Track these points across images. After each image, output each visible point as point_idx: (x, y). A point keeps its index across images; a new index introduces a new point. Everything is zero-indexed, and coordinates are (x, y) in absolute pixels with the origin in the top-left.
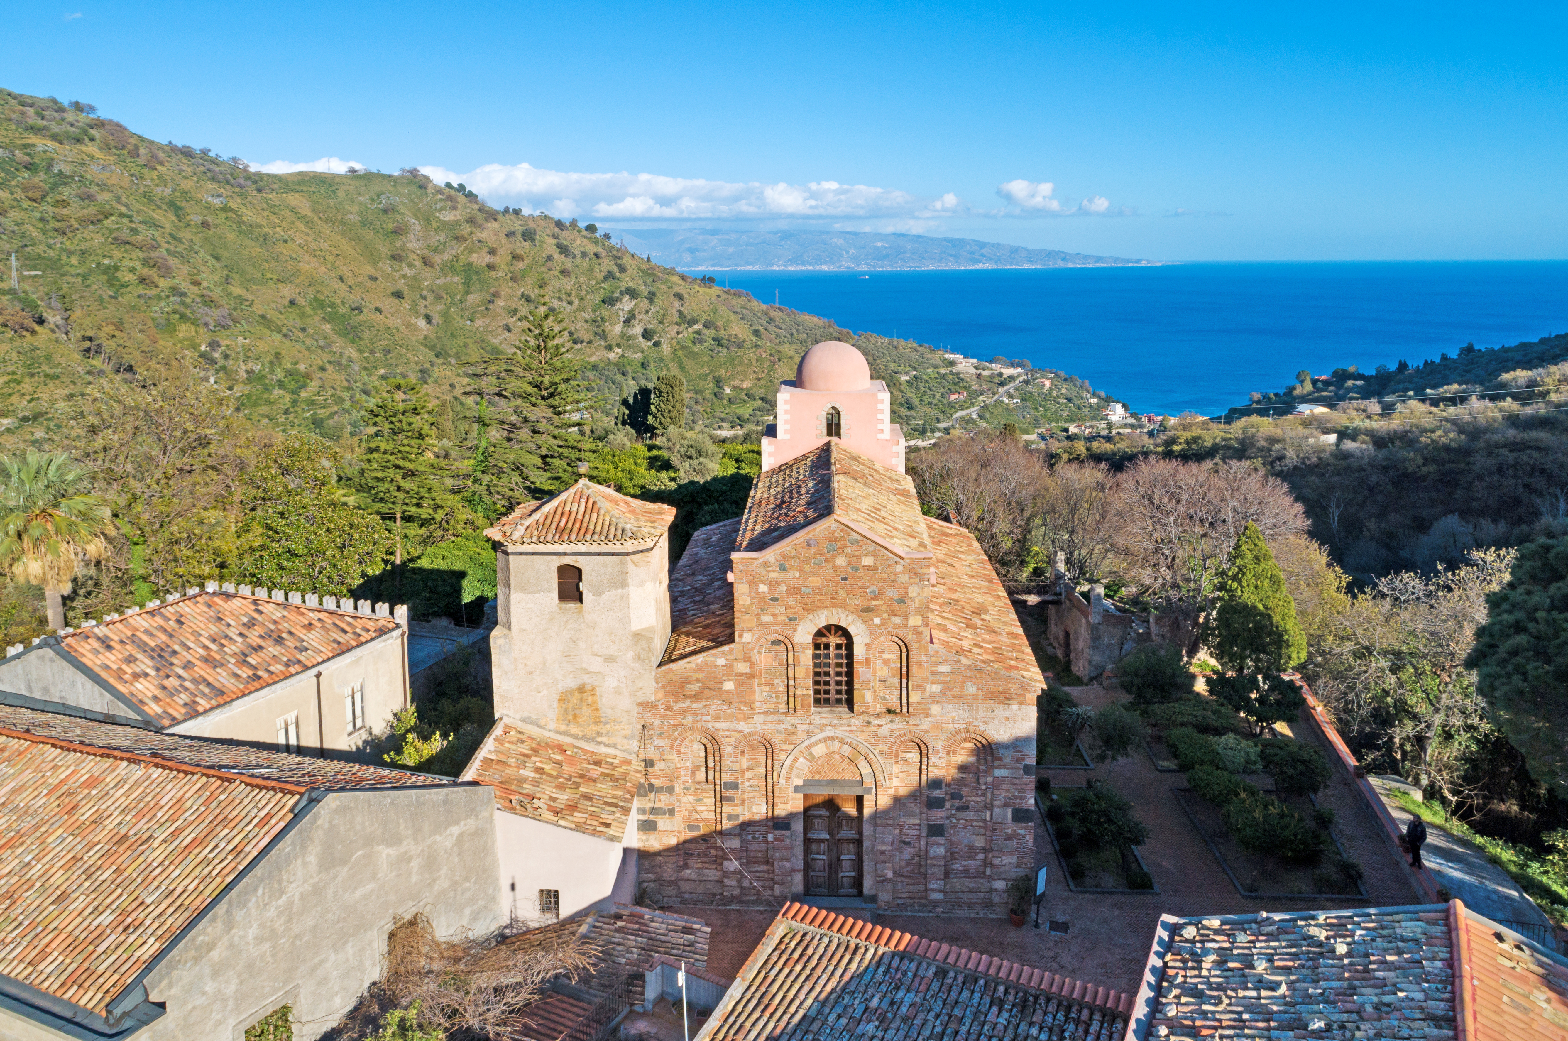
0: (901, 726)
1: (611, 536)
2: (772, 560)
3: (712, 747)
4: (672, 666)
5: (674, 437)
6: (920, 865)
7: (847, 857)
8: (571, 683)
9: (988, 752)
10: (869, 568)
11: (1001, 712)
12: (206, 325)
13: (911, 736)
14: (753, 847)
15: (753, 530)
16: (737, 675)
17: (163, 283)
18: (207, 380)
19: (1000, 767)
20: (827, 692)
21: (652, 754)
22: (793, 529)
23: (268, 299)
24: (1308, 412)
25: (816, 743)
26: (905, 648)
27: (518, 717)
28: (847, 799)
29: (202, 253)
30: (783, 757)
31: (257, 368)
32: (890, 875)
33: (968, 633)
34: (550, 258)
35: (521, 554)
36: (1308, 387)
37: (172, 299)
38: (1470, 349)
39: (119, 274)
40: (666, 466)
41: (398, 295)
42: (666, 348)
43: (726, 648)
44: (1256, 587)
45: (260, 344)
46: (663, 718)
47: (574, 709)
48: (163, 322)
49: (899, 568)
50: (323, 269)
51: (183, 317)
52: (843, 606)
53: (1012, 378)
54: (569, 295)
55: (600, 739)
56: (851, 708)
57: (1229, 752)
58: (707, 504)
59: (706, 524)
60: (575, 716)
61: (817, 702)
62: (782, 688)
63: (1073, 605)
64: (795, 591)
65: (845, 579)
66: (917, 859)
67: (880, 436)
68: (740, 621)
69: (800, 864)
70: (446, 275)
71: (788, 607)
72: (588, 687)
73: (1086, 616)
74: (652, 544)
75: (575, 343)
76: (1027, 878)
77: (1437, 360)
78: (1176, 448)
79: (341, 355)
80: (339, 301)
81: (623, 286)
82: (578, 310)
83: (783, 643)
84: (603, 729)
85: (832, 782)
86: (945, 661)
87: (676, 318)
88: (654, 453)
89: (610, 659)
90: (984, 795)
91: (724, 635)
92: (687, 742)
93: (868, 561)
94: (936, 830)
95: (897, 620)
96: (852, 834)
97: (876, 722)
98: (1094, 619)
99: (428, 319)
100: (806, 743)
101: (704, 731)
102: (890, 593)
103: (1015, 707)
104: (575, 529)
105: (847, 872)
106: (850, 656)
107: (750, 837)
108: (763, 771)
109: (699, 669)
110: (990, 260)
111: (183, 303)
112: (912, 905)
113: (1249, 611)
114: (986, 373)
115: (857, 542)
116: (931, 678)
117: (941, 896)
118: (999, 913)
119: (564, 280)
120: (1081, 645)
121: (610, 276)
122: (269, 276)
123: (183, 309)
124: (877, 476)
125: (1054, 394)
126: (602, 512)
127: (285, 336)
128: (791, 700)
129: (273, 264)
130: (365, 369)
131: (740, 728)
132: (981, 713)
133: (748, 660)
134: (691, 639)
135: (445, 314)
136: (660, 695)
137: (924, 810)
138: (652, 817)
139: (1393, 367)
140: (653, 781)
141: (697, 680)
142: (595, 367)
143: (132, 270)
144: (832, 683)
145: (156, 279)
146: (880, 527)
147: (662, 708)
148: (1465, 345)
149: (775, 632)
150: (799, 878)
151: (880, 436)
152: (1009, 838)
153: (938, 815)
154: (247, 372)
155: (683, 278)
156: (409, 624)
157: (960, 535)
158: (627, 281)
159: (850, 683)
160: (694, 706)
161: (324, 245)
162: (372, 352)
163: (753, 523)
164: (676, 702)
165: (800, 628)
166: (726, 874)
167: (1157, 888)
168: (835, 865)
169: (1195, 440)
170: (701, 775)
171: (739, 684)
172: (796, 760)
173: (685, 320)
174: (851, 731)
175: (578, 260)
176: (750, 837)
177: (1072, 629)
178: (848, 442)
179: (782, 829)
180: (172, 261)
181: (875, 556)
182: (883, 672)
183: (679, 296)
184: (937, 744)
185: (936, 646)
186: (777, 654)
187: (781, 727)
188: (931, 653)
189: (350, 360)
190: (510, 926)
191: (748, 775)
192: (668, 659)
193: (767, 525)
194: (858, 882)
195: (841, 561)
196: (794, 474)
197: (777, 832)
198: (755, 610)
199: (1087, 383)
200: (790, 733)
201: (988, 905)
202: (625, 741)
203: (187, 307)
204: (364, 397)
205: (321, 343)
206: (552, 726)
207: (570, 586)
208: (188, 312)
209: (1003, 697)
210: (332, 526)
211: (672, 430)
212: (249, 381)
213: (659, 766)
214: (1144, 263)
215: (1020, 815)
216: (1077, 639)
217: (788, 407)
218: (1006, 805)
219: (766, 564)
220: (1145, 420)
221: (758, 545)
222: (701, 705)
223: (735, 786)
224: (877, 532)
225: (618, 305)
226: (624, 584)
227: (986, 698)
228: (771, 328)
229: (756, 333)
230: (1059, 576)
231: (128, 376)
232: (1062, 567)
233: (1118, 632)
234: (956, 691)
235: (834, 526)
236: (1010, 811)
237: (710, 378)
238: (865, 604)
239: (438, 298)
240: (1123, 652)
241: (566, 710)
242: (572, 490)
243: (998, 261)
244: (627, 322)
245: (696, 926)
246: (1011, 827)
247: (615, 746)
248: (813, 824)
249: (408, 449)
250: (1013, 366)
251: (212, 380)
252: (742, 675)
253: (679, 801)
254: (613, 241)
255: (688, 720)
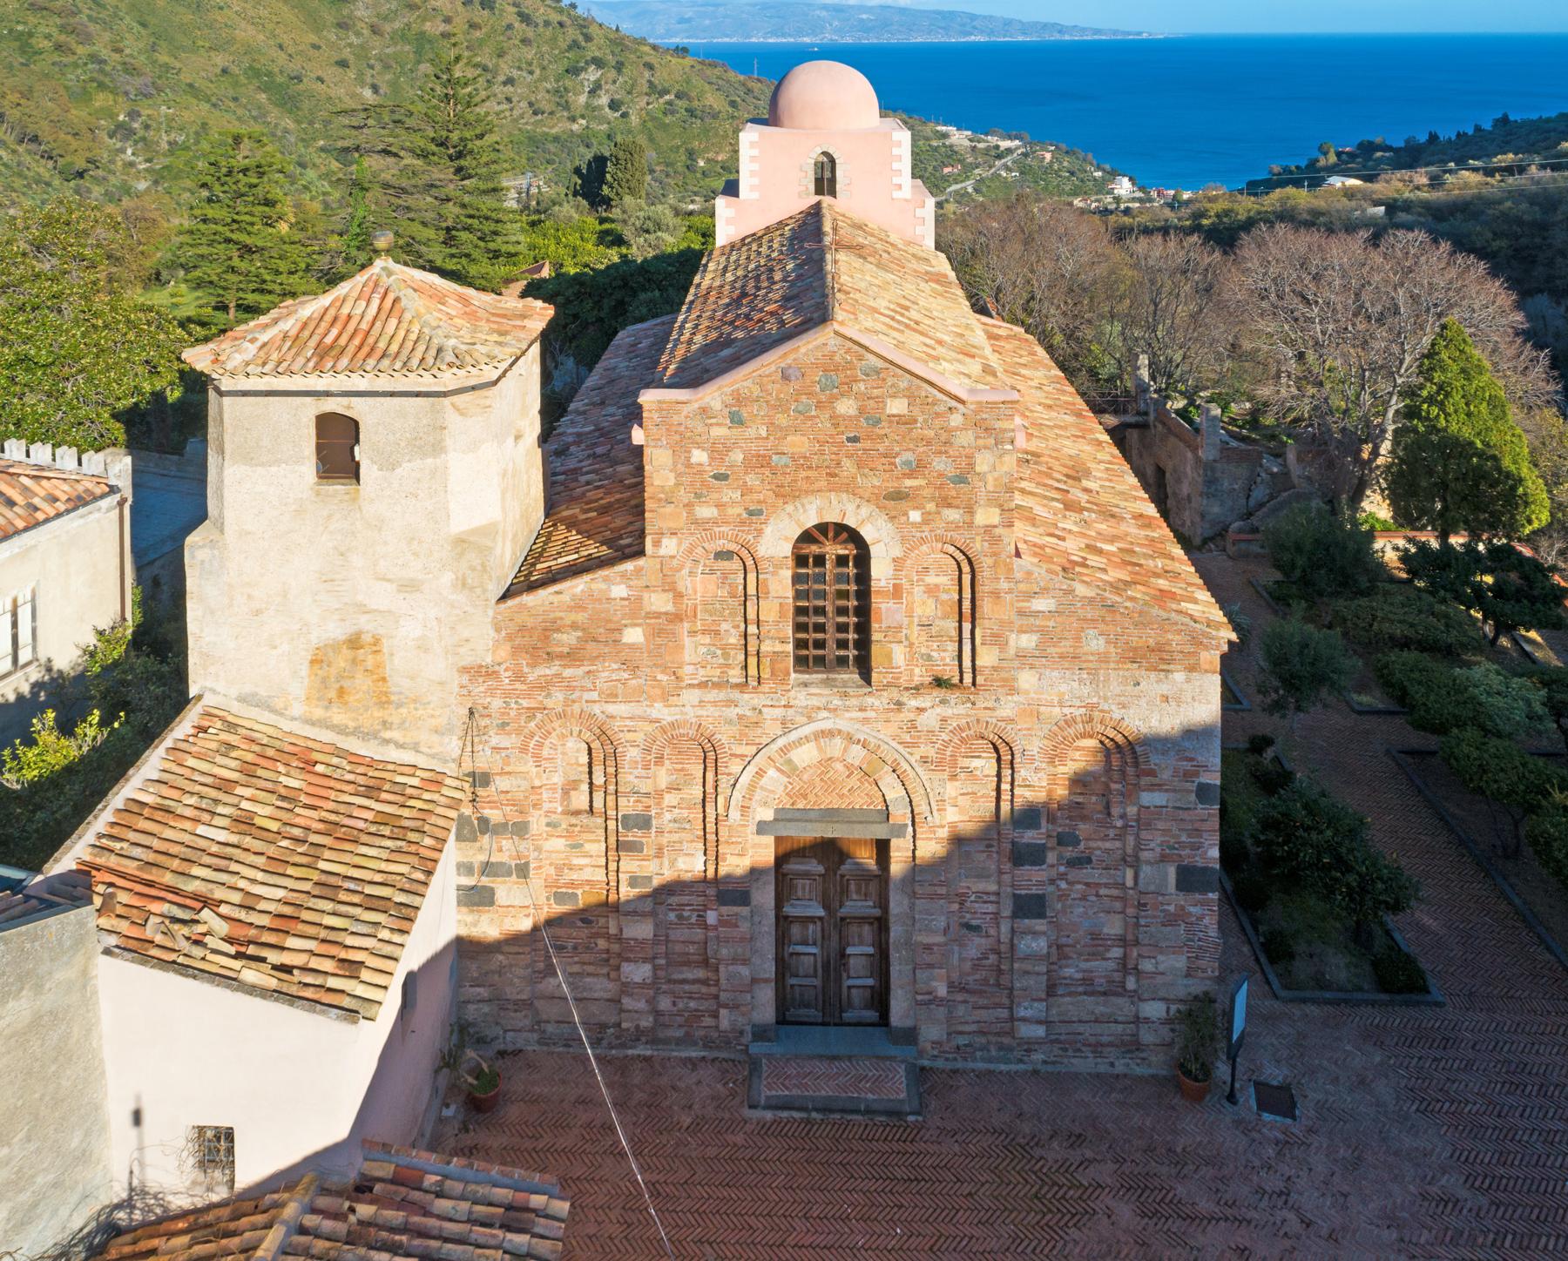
0: (961, 710)
1: (415, 362)
2: (716, 405)
3: (603, 751)
4: (528, 599)
5: (630, 208)
6: (1000, 972)
7: (860, 950)
8: (336, 631)
9: (1128, 759)
10: (900, 420)
11: (1152, 685)
12: (126, 93)
13: (976, 729)
14: (678, 934)
15: (690, 342)
16: (649, 615)
17: (80, 50)
18: (123, 151)
19: (1152, 788)
20: (820, 644)
21: (485, 761)
22: (759, 346)
23: (198, 67)
24: (1339, 185)
25: (799, 742)
26: (968, 568)
27: (234, 692)
28: (858, 842)
29: (128, 19)
30: (735, 768)
31: (181, 139)
32: (942, 991)
33: (1069, 523)
34: (510, 27)
35: (245, 394)
36: (1333, 159)
37: (90, 66)
38: (1505, 120)
39: (33, 41)
40: (619, 241)
41: (343, 64)
42: (634, 119)
43: (629, 566)
44: (1469, 415)
45: (186, 114)
46: (506, 695)
47: (339, 678)
48: (78, 90)
49: (956, 420)
50: (261, 37)
51: (101, 86)
52: (850, 489)
53: (1009, 151)
54: (530, 64)
55: (387, 735)
56: (866, 675)
57: (1499, 702)
58: (645, 290)
59: (642, 320)
60: (341, 692)
61: (801, 662)
62: (734, 639)
63: (1169, 429)
64: (759, 462)
65: (854, 440)
66: (993, 958)
67: (897, 194)
68: (656, 518)
69: (769, 969)
70: (396, 44)
71: (746, 491)
72: (367, 638)
73: (1195, 450)
74: (495, 375)
75: (535, 113)
76: (1207, 999)
77: (1470, 132)
78: (1205, 222)
79: (276, 125)
80: (276, 70)
81: (589, 55)
82: (541, 80)
83: (739, 558)
84: (394, 716)
85: (830, 815)
86: (1044, 591)
87: (645, 89)
88: (606, 226)
89: (409, 587)
90: (1120, 837)
91: (626, 543)
92: (553, 739)
93: (897, 407)
94: (1029, 906)
95: (953, 515)
96: (867, 907)
97: (914, 703)
98: (1207, 453)
99: (375, 89)
100: (781, 742)
101: (586, 718)
102: (940, 464)
103: (1179, 676)
104: (351, 349)
105: (858, 978)
106: (864, 578)
107: (672, 916)
108: (697, 792)
109: (578, 606)
110: (982, 32)
111: (101, 71)
112: (983, 1048)
113: (1457, 449)
114: (981, 145)
115: (878, 372)
116: (1018, 621)
117: (1040, 1031)
118: (1156, 1064)
119: (525, 49)
120: (1185, 489)
121: (574, 45)
122: (200, 43)
123: (101, 78)
124: (896, 254)
125: (1056, 167)
126: (408, 316)
127: (214, 105)
128: (752, 661)
129: (206, 31)
130: (303, 140)
131: (655, 714)
132: (1114, 687)
133: (671, 588)
134: (574, 536)
135: (394, 84)
136: (504, 652)
137: (1007, 866)
138: (485, 881)
139: (1423, 138)
140: (487, 812)
141: (574, 626)
142: (556, 139)
143: (48, 37)
144: (830, 628)
145: (74, 46)
146: (914, 341)
147: (505, 677)
148: (1500, 116)
149: (722, 536)
150: (766, 995)
151: (897, 194)
152: (1171, 920)
153: (1033, 878)
154: (170, 143)
155: (655, 47)
156: (136, 486)
157: (1014, 337)
158: (593, 51)
159: (864, 629)
160: (568, 672)
161: (264, 13)
162: (311, 123)
163: (691, 329)
164: (533, 666)
165: (768, 530)
166: (626, 988)
167: (1436, 994)
168: (835, 964)
169: (1227, 213)
170: (580, 799)
171: (655, 633)
172: (760, 773)
173: (655, 90)
174: (866, 721)
175: (541, 29)
176: (672, 916)
177: (1169, 467)
178: (845, 205)
179: (735, 903)
180: (93, 28)
181: (911, 398)
182: (926, 608)
183: (650, 67)
184: (1031, 744)
185: (1028, 560)
186: (725, 576)
187: (732, 712)
188: (1018, 575)
189: (286, 131)
190: (127, 1204)
191: (671, 799)
192: (524, 583)
193: (714, 335)
194: (880, 999)
195: (846, 407)
196: (764, 250)
197: (725, 910)
198: (684, 496)
199: (1090, 156)
200: (750, 724)
201: (1133, 1046)
202: (435, 738)
203: (106, 75)
204: (299, 170)
205: (254, 113)
206: (297, 709)
207: (337, 450)
208: (107, 80)
209: (1157, 658)
210: (100, 323)
211: (628, 199)
212: (171, 152)
213: (501, 783)
214: (1145, 36)
215: (1189, 879)
216: (1179, 481)
217: (755, 152)
218: (1164, 859)
219: (704, 411)
220: (1154, 194)
221: (694, 375)
222: (580, 671)
223: (644, 822)
224: (907, 350)
225: (583, 75)
226: (438, 449)
227: (1123, 659)
228: (750, 99)
229: (733, 104)
230: (1144, 389)
231: (33, 147)
232: (1145, 374)
233: (1242, 471)
234: (1066, 646)
235: (834, 342)
236: (1172, 872)
237: (682, 150)
238: (891, 485)
239: (387, 67)
240: (1252, 502)
241: (324, 681)
242: (360, 278)
243: (992, 32)
244: (592, 92)
245: (537, 1200)
246: (1175, 900)
247: (416, 748)
248: (792, 887)
249: (247, 218)
250: (1010, 138)
251: (129, 151)
252: (658, 615)
253: (538, 849)
254: (580, 11)
255: (556, 699)
